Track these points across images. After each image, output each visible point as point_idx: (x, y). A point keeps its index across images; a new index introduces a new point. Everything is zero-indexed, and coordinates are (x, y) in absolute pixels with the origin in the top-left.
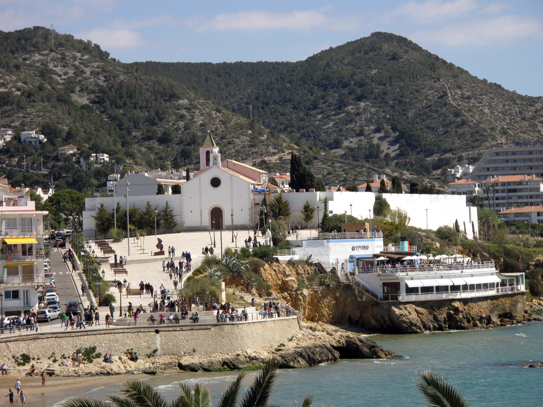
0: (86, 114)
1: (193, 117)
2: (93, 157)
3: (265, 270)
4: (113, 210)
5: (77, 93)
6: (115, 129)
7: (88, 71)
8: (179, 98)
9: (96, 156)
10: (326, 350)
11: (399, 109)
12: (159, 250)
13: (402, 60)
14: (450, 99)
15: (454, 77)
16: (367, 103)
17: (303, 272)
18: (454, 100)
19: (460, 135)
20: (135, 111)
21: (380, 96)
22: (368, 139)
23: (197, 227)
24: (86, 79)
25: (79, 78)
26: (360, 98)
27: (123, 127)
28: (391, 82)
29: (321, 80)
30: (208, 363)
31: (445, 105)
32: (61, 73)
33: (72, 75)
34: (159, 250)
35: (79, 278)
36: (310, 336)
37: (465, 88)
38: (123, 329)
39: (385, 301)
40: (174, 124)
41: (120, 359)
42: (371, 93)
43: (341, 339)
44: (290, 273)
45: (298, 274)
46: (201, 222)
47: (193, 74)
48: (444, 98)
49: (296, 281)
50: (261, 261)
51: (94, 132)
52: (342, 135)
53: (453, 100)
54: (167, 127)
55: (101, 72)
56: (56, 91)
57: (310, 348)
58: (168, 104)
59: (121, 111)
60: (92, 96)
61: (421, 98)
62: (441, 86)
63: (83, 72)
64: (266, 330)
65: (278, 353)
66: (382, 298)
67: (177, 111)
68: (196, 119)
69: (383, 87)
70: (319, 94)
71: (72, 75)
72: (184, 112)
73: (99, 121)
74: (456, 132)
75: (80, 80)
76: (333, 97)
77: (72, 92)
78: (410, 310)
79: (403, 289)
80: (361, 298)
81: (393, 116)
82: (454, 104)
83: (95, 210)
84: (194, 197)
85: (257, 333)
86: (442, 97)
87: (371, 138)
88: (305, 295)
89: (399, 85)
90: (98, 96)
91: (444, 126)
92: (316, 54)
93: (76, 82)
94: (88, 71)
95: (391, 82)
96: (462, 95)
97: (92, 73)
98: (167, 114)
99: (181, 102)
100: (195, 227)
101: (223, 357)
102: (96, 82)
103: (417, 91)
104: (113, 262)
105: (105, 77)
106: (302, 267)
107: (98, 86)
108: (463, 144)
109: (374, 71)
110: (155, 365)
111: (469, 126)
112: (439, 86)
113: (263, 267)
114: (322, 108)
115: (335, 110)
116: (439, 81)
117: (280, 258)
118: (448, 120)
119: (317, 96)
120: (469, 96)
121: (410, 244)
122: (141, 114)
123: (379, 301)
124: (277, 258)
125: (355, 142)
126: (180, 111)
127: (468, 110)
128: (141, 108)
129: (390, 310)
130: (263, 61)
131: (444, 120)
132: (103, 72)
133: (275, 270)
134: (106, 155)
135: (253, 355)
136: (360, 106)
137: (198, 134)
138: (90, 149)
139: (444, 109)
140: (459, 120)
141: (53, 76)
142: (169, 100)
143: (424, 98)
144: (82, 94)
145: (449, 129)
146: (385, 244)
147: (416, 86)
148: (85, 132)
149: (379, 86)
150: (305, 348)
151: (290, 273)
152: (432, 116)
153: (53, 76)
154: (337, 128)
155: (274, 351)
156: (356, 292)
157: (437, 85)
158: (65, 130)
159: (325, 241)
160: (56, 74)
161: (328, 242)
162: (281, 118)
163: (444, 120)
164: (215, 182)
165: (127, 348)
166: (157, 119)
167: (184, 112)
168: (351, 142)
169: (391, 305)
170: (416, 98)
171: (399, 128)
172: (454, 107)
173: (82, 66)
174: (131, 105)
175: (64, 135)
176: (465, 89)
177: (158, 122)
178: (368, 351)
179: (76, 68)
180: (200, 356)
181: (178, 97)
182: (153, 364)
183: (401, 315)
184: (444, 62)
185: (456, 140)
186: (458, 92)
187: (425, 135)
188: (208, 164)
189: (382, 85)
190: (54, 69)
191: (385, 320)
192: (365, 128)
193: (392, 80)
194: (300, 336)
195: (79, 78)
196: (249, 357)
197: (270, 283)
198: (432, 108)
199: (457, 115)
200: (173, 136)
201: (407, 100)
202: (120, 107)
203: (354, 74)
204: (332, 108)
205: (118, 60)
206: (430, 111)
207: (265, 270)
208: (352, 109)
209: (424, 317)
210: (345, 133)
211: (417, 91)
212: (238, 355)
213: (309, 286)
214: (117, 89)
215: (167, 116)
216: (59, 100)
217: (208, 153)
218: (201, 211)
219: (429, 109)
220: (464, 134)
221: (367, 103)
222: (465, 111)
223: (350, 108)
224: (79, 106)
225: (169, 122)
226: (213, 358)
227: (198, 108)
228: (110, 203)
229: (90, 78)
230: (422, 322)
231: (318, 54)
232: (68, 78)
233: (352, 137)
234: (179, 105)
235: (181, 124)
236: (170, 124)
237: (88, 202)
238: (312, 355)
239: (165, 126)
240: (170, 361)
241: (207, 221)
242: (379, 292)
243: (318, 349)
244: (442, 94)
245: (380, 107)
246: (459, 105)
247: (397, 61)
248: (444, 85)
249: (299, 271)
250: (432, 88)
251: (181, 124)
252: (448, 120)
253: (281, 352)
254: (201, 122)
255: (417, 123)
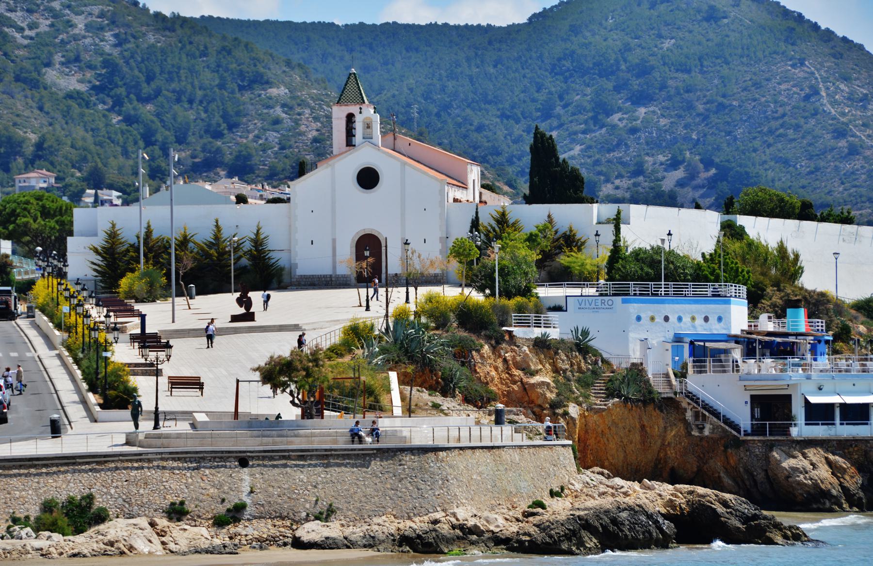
0: (76, 109)
1: (297, 123)
2: (89, 196)
3: (482, 357)
4: (138, 237)
5: (57, 66)
6: (136, 143)
7: (80, 22)
8: (268, 83)
9: (96, 195)
10: (643, 518)
11: (717, 121)
12: (242, 311)
13: (726, 21)
14: (825, 101)
15: (834, 56)
16: (652, 109)
17: (567, 366)
18: (834, 103)
19: (845, 174)
20: (176, 107)
21: (679, 94)
22: (652, 181)
23: (325, 276)
24: (76, 38)
25: (61, 37)
26: (641, 99)
27: (153, 139)
28: (702, 66)
29: (559, 60)
30: (364, 537)
31: (815, 113)
32: (24, 25)
33: (47, 29)
34: (242, 311)
35: (57, 362)
36: (602, 489)
37: (857, 79)
38: (162, 453)
39: (756, 438)
40: (258, 137)
41: (153, 524)
42: (661, 89)
43: (676, 496)
44: (540, 367)
45: (556, 370)
46: (334, 268)
47: (296, 44)
48: (813, 99)
49: (552, 384)
50: (474, 337)
51: (92, 147)
52: (600, 173)
53: (831, 103)
54: (245, 141)
55: (108, 25)
56: (13, 61)
57: (607, 512)
58: (247, 96)
59: (149, 107)
60: (89, 75)
61: (763, 99)
62: (806, 75)
63: (70, 24)
64: (501, 468)
65: (531, 519)
66: (749, 431)
67: (265, 111)
68: (303, 128)
69: (686, 76)
70: (553, 89)
71: (47, 29)
72: (278, 111)
73: (101, 125)
74: (836, 168)
75: (62, 40)
76: (582, 95)
77: (48, 64)
78: (814, 459)
79: (798, 410)
80: (701, 429)
81: (705, 135)
82: (833, 112)
83: (96, 235)
84: (315, 217)
85: (480, 474)
86: (807, 98)
87: (658, 180)
88: (572, 418)
89: (719, 71)
90: (100, 75)
91: (810, 158)
92: (548, 7)
93: (54, 46)
94: (80, 22)
95: (702, 66)
96: (851, 93)
97: (88, 27)
98: (245, 116)
99: (274, 91)
100: (320, 277)
101: (401, 526)
102: (96, 45)
103: (757, 85)
104: (138, 331)
105: (116, 36)
106: (567, 356)
107: (101, 55)
108: (850, 195)
109: (668, 44)
110: (237, 541)
111: (865, 158)
112: (802, 75)
113: (478, 351)
114: (559, 117)
115: (586, 122)
116: (802, 64)
117: (518, 332)
118: (819, 145)
119: (550, 93)
120: (866, 95)
121: (810, 315)
122: (189, 115)
123: (742, 437)
124: (510, 333)
125: (626, 186)
126: (272, 111)
127: (864, 125)
128: (191, 102)
129: (767, 458)
130: (439, 23)
131: (810, 145)
132: (112, 27)
133: (505, 361)
134: (115, 193)
135: (471, 522)
136: (637, 114)
137: (308, 157)
138: (84, 179)
139: (813, 122)
140: (843, 143)
141: (6, 29)
142: (249, 87)
143: (769, 98)
144: (68, 70)
145: (822, 164)
146: (753, 315)
147: (755, 74)
148: (72, 146)
149: (676, 75)
150: (599, 513)
151: (540, 367)
152: (785, 135)
153: (6, 29)
154: (590, 157)
155: (520, 517)
156: (689, 415)
157: (799, 73)
158: (30, 139)
159: (619, 299)
160: (11, 26)
161: (624, 302)
162: (475, 136)
163: (810, 145)
164: (368, 178)
165: (171, 498)
166: (224, 126)
167: (278, 111)
168: (617, 188)
169: (771, 446)
170: (755, 100)
171: (717, 160)
172: (833, 119)
173: (67, 11)
174: (170, 95)
175: (29, 150)
176: (857, 82)
177: (226, 132)
178: (739, 525)
179: (56, 15)
180: (343, 522)
181: (267, 82)
182: (231, 538)
183: (795, 469)
184: (815, 27)
185: (836, 184)
186: (842, 86)
187: (770, 174)
188: (350, 143)
189: (682, 71)
190: (8, 15)
191: (755, 481)
192: (647, 158)
193: (705, 63)
194: (578, 486)
195: (61, 37)
196: (462, 527)
197: (494, 388)
198: (786, 118)
199: (840, 133)
200: (255, 160)
201: (734, 103)
202: (147, 100)
203: (627, 48)
204: (582, 117)
205: (144, 5)
206: (782, 126)
207: (482, 357)
208: (620, 120)
209: (847, 478)
210: (604, 169)
211: (757, 85)
212: (436, 522)
213: (581, 399)
214: (143, 61)
215: (244, 120)
216: (17, 79)
217: (350, 118)
218: (334, 241)
219: (780, 121)
220: (853, 173)
221: (652, 109)
222: (855, 126)
223: (616, 117)
224: (61, 94)
225: (249, 132)
226: (376, 528)
227: (308, 106)
228: (130, 220)
229: (84, 37)
230: (843, 488)
231: (552, 7)
232: (37, 34)
233: (620, 176)
234: (270, 98)
235: (273, 136)
236: (251, 136)
237: (80, 216)
238: (611, 528)
239: (240, 140)
240: (273, 531)
241: (345, 261)
242: (742, 415)
243: (624, 515)
244: (807, 91)
245: (680, 116)
246: (843, 114)
247: (716, 22)
248: (813, 73)
249: (560, 365)
250: (785, 79)
251: (273, 136)
252: (819, 145)
253: (538, 518)
254: (315, 133)
255: (755, 150)
